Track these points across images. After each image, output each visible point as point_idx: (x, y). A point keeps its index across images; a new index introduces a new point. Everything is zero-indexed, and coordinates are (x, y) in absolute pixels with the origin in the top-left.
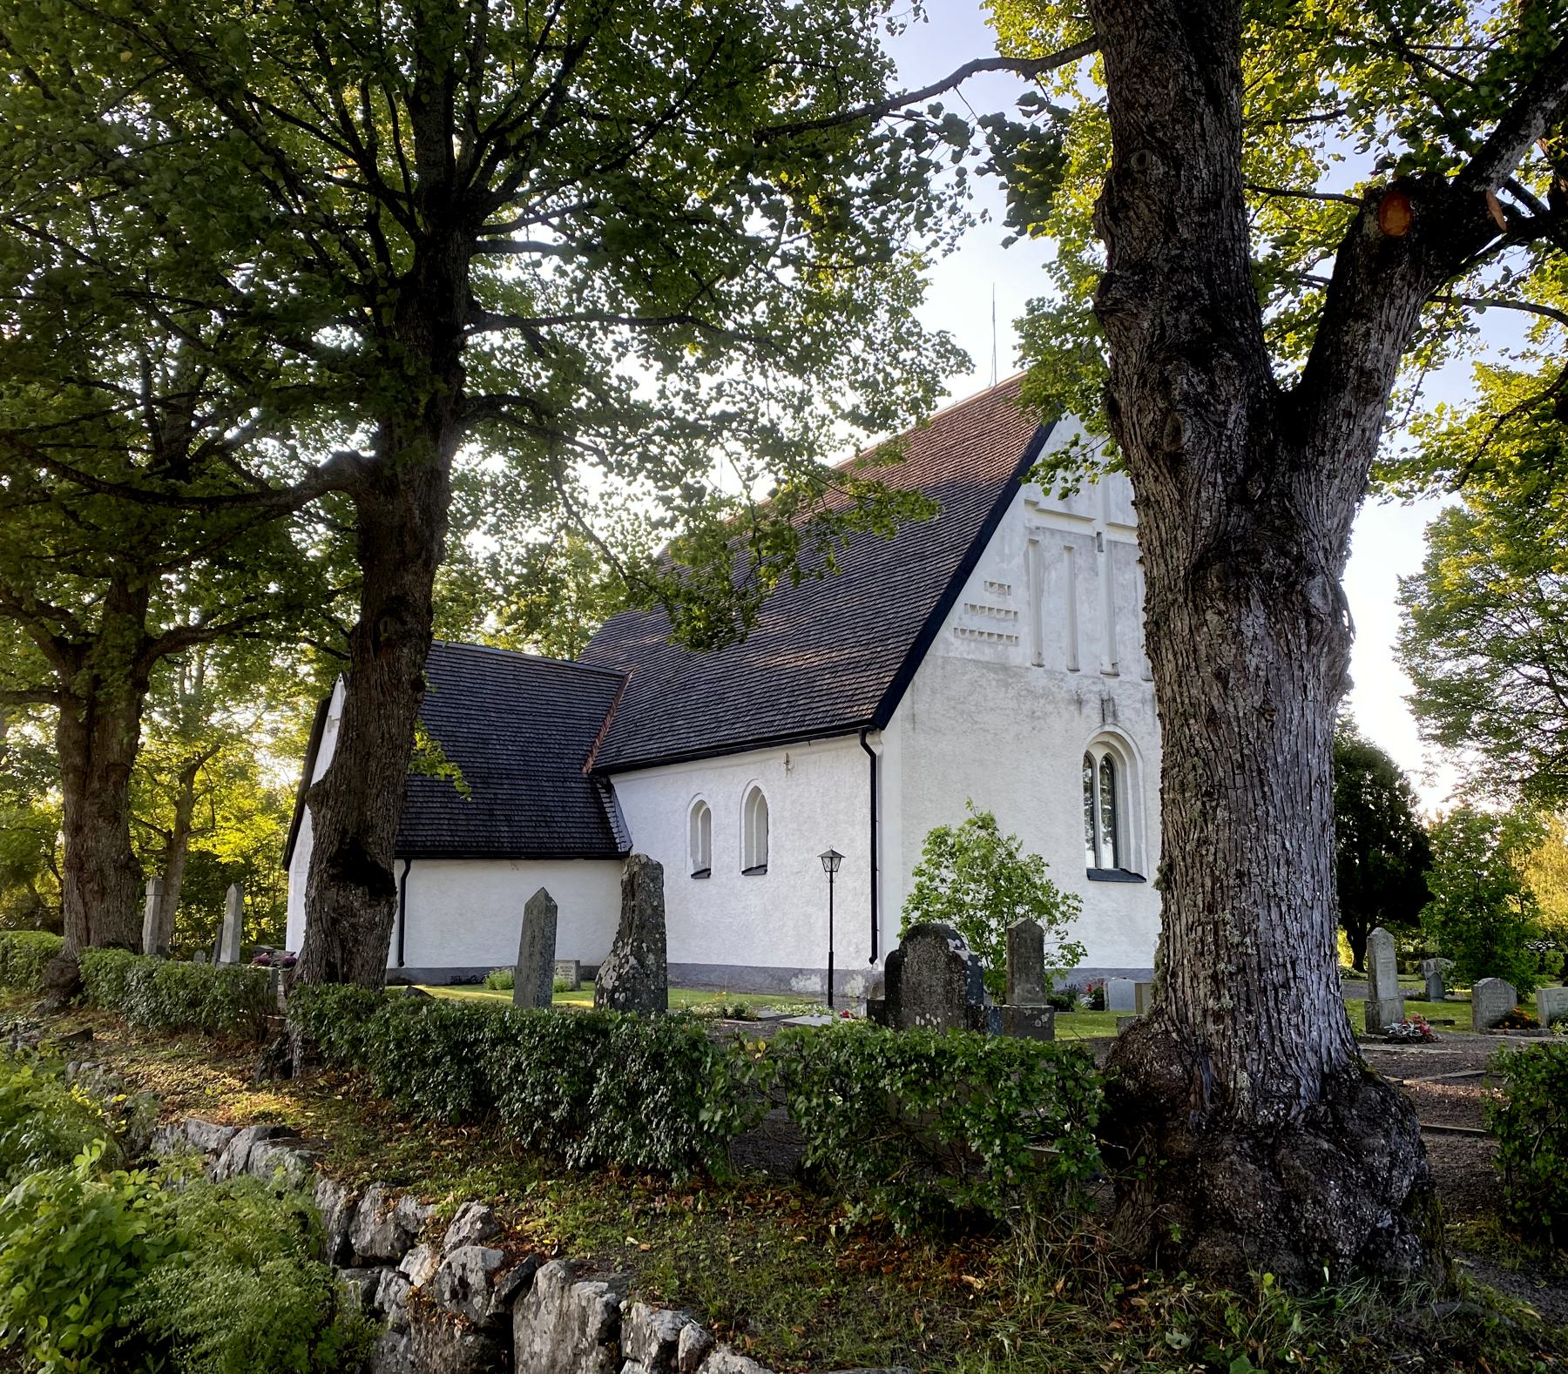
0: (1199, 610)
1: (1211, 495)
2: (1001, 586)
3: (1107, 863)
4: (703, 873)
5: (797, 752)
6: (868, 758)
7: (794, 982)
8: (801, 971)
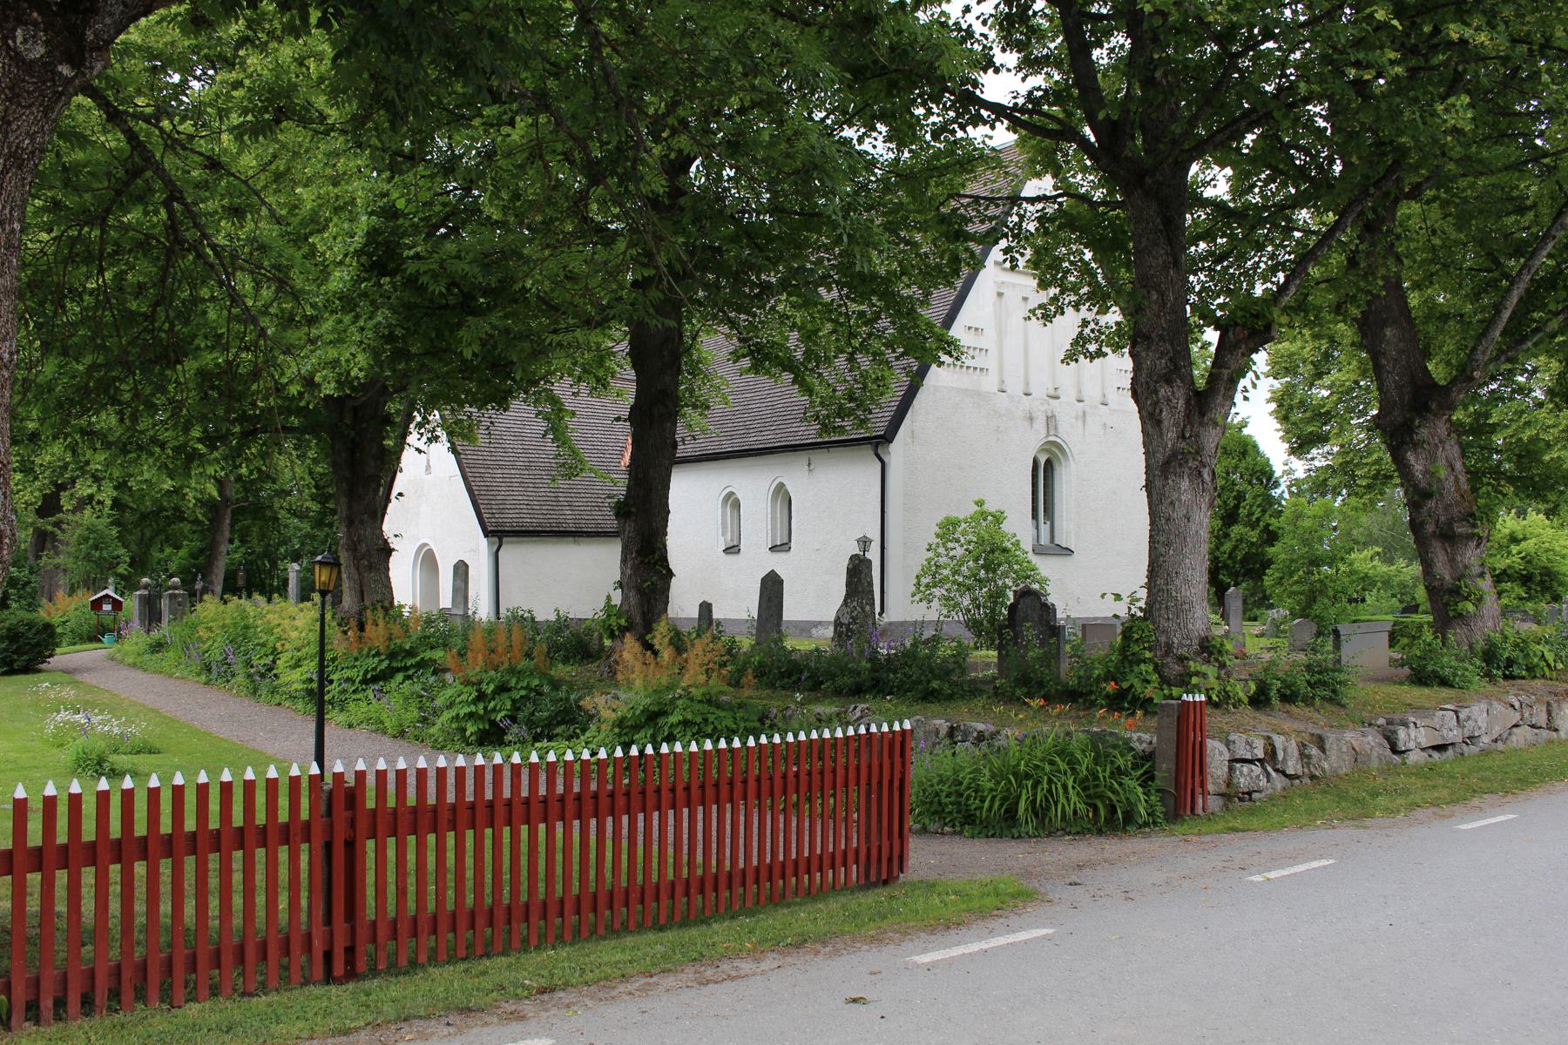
0: (1167, 478)
1: (1171, 435)
2: (977, 329)
3: (1045, 540)
4: (732, 550)
5: (818, 456)
7: (814, 631)
8: (820, 623)
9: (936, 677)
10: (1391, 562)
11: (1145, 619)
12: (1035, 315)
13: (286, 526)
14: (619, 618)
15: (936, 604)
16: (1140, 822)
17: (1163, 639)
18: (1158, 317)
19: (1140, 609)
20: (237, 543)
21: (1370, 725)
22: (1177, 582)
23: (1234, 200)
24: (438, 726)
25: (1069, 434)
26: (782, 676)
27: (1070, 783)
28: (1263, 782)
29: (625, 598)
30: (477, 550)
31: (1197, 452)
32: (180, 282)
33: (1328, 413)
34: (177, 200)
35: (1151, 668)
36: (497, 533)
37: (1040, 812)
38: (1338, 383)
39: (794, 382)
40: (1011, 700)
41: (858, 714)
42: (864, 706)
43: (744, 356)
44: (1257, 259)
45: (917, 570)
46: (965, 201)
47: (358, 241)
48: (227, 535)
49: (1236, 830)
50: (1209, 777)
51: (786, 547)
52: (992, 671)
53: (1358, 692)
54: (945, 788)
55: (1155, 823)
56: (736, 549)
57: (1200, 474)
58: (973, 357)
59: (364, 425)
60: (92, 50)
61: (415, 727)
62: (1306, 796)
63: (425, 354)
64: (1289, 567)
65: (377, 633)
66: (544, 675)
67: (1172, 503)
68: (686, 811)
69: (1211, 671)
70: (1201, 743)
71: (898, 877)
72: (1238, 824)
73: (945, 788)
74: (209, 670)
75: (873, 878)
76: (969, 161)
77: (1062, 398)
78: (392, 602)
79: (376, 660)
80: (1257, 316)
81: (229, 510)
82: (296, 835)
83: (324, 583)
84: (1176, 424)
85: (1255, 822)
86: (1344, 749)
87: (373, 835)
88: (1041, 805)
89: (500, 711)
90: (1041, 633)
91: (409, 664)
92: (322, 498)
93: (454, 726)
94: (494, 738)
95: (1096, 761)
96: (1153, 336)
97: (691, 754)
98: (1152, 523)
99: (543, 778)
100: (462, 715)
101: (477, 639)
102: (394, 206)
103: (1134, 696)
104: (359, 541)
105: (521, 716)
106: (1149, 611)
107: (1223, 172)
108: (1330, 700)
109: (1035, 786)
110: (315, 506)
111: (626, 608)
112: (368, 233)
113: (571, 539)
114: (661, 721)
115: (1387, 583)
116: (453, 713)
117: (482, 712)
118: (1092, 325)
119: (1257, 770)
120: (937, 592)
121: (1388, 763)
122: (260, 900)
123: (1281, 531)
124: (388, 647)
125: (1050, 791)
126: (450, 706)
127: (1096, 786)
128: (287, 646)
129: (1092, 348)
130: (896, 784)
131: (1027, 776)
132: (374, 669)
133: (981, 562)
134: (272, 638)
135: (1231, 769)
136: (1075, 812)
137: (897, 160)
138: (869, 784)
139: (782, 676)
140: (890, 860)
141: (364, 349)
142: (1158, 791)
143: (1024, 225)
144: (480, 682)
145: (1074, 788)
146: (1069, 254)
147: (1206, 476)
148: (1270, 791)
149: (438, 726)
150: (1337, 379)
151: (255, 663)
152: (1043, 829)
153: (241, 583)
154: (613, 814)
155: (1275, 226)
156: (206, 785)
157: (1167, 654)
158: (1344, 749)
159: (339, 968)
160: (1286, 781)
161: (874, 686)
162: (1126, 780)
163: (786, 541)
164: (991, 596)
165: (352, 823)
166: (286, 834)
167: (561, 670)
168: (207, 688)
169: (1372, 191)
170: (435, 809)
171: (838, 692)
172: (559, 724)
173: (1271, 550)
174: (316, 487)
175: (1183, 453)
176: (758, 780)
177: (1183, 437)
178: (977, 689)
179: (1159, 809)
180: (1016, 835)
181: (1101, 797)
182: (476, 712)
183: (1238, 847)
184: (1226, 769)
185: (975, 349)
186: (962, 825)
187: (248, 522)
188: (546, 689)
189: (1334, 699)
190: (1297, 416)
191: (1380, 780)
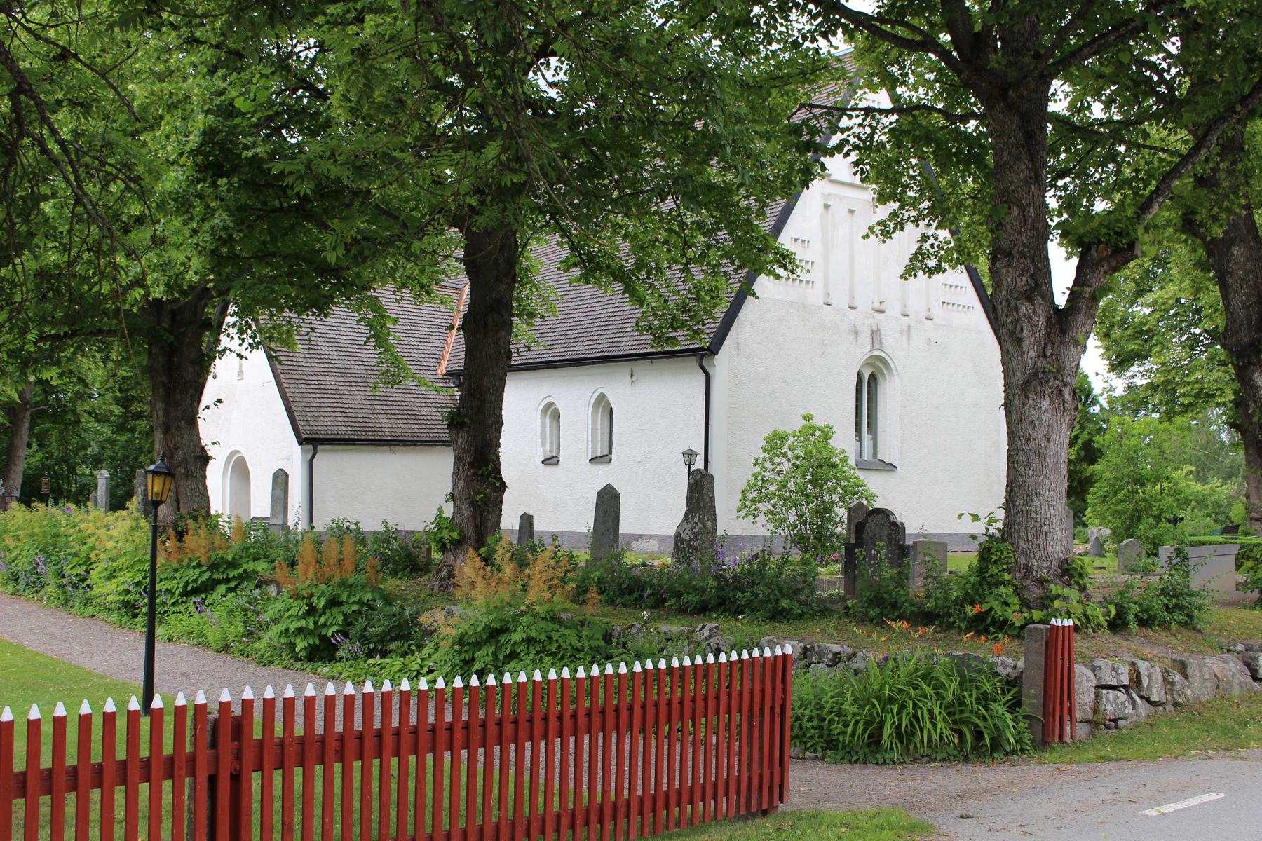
1: (1031, 354)
2: (803, 241)
3: (867, 455)
4: (552, 461)
5: (639, 366)
8: (641, 536)
9: (785, 596)
10: (1203, 481)
12: (873, 232)
13: (86, 430)
14: (452, 530)
15: (762, 519)
17: (1022, 561)
18: (1019, 233)
19: (999, 529)
20: (35, 447)
21: (1229, 651)
22: (1037, 503)
24: (265, 640)
25: (893, 349)
26: (623, 592)
27: (936, 710)
29: (457, 510)
30: (292, 457)
31: (1058, 371)
32: (22, 179)
33: (1150, 330)
34: (24, 92)
35: (1010, 590)
36: (311, 441)
37: (904, 738)
38: (1160, 301)
39: (624, 293)
40: (863, 621)
41: (706, 633)
42: (713, 625)
43: (575, 265)
45: (744, 485)
46: (817, 111)
47: (194, 140)
48: (26, 438)
49: (1109, 759)
52: (839, 590)
53: (1213, 617)
54: (807, 712)
55: (1022, 750)
56: (555, 460)
57: (1061, 393)
58: (808, 271)
59: (182, 330)
61: (240, 642)
62: (1172, 723)
63: (252, 257)
64: (1114, 486)
65: (196, 541)
66: (375, 589)
67: (1032, 423)
68: (572, 739)
69: (1072, 593)
70: (1069, 668)
71: (777, 807)
72: (1108, 751)
73: (807, 712)
74: (17, 580)
75: (754, 809)
76: (813, 71)
77: (887, 313)
78: (208, 512)
79: (197, 571)
80: (1120, 234)
81: (28, 413)
82: (181, 768)
83: (157, 494)
84: (1037, 342)
85: (1126, 751)
86: (1207, 676)
87: (260, 767)
88: (906, 732)
89: (331, 625)
91: (231, 576)
92: (125, 402)
93: (282, 641)
94: (324, 654)
96: (1014, 252)
97: (578, 680)
98: (1011, 442)
99: (431, 705)
100: (291, 630)
103: (993, 618)
104: (176, 448)
105: (352, 631)
106: (1007, 533)
108: (1186, 624)
109: (899, 713)
110: (118, 410)
111: (458, 520)
112: (204, 132)
114: (503, 638)
115: (1201, 502)
116: (282, 627)
117: (312, 627)
118: (932, 241)
119: (1122, 696)
120: (763, 507)
121: (1249, 691)
124: (209, 558)
125: (915, 716)
126: (276, 621)
127: (961, 712)
128: (102, 556)
129: (932, 263)
130: (778, 710)
132: (195, 581)
133: (809, 477)
134: (85, 547)
135: (1097, 695)
136: (942, 738)
138: (751, 710)
140: (771, 788)
141: (200, 252)
142: (1025, 717)
143: (876, 137)
144: (312, 595)
147: (1067, 395)
148: (1135, 718)
149: (265, 640)
150: (1160, 297)
151: (67, 572)
152: (908, 755)
153: (44, 489)
154: (500, 744)
156: (89, 717)
157: (1026, 576)
158: (1207, 676)
160: (1152, 708)
161: (720, 605)
162: (995, 706)
164: (818, 512)
165: (239, 755)
166: (170, 768)
167: (391, 585)
168: (14, 599)
169: (1239, 108)
170: (323, 740)
171: (682, 611)
172: (393, 639)
173: (1096, 467)
174: (120, 390)
175: (1044, 372)
176: (644, 707)
177: (1044, 356)
178: (827, 609)
179: (1027, 736)
180: (881, 761)
182: (306, 628)
184: (1093, 696)
185: (807, 262)
186: (824, 750)
187: (47, 425)
188: (379, 604)
189: (1189, 624)
191: (1243, 709)
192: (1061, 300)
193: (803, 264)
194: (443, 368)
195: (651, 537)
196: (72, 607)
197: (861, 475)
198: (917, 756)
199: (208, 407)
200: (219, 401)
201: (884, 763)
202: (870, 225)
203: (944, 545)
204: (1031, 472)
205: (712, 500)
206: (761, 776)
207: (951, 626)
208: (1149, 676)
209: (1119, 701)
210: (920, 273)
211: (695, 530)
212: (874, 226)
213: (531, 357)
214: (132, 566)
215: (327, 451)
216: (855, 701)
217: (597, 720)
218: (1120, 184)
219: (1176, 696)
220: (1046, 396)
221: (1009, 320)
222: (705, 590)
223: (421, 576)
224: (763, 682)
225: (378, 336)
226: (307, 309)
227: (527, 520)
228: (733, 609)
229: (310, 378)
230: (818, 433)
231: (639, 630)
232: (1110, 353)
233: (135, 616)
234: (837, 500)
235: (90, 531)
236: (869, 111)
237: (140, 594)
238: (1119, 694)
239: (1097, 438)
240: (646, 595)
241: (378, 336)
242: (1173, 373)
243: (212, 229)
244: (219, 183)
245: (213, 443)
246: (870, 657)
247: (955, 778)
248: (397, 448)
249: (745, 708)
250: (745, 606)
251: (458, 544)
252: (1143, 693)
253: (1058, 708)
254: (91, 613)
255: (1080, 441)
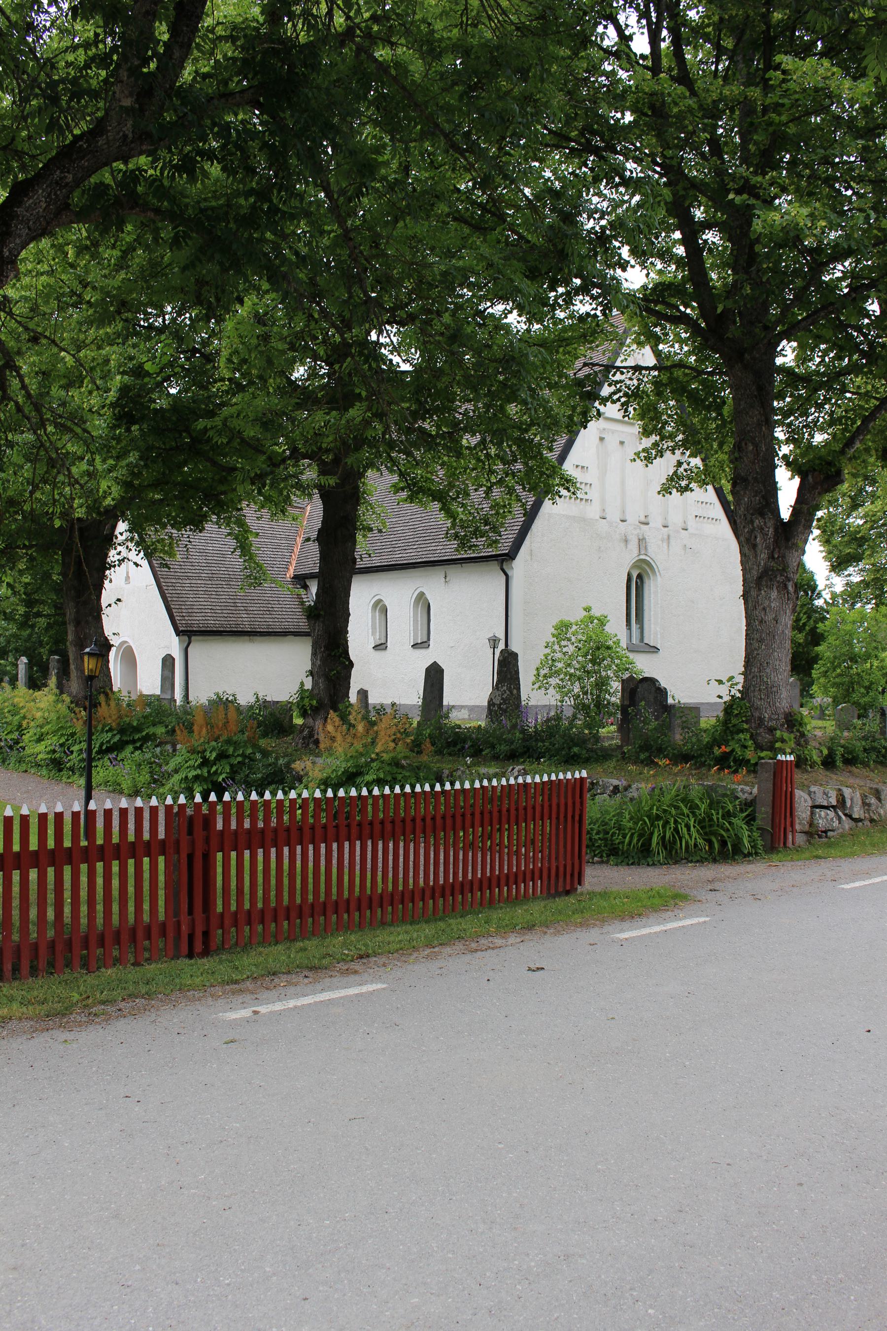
0: (760, 590)
1: (763, 556)
2: (583, 467)
4: (380, 647)
5: (452, 570)
6: (504, 577)
9: (576, 745)
11: (742, 699)
12: (639, 457)
15: (551, 691)
16: (746, 852)
17: (757, 714)
19: (739, 690)
22: (768, 670)
23: (798, 366)
25: (656, 553)
26: (449, 745)
27: (692, 823)
28: (836, 824)
29: (315, 684)
30: (173, 645)
31: (784, 570)
33: (862, 538)
38: (871, 513)
39: (441, 510)
42: (521, 767)
43: (403, 489)
44: (817, 415)
45: (537, 664)
47: (112, 395)
50: (797, 819)
51: (426, 645)
52: (617, 742)
55: (756, 854)
56: (384, 646)
57: (786, 587)
60: (8, 263)
67: (764, 609)
75: (561, 889)
78: (111, 689)
79: (110, 735)
83: (92, 670)
84: (767, 547)
89: (221, 773)
90: (655, 711)
91: (136, 737)
92: (30, 603)
93: (183, 786)
95: (711, 806)
96: (750, 478)
101: (199, 719)
102: (142, 368)
103: (735, 758)
105: (238, 777)
106: (745, 692)
107: (790, 344)
109: (664, 827)
110: (22, 610)
111: (316, 692)
113: (247, 638)
117: (206, 774)
118: (685, 466)
119: (831, 814)
120: (554, 681)
122: (100, 908)
123: (826, 634)
125: (676, 830)
126: (176, 771)
127: (711, 826)
128: (32, 724)
130: (577, 818)
131: (658, 818)
132: (108, 742)
133: (589, 657)
134: (17, 717)
135: (812, 813)
137: (528, 331)
138: (558, 818)
139: (449, 745)
140: (572, 875)
142: (758, 829)
144: (205, 750)
145: (694, 827)
146: (667, 409)
147: (791, 588)
148: (841, 830)
150: (870, 510)
152: (671, 858)
155: (830, 388)
159: (199, 947)
160: (854, 823)
161: (525, 753)
162: (734, 820)
163: (425, 639)
164: (597, 685)
165: (207, 840)
171: (496, 758)
173: (819, 649)
175: (773, 570)
177: (773, 558)
179: (760, 842)
180: (651, 863)
181: (715, 834)
183: (824, 868)
184: (809, 813)
185: (586, 484)
186: (608, 856)
188: (258, 756)
190: (838, 539)
192: (785, 514)
193: (583, 486)
194: (291, 573)
195: (462, 707)
196: (9, 764)
197: (631, 656)
198: (678, 859)
199: (110, 605)
200: (119, 600)
201: (654, 864)
202: (636, 451)
203: (699, 708)
204: (763, 647)
205: (517, 672)
206: (565, 866)
207: (703, 764)
208: (852, 799)
209: (829, 818)
210: (674, 491)
211: (504, 696)
212: (639, 453)
213: (376, 562)
214: (58, 730)
215: (199, 641)
216: (631, 818)
217: (449, 822)
218: (832, 422)
219: (872, 814)
220: (775, 588)
221: (746, 530)
222: (514, 741)
223: (287, 736)
224: (566, 798)
225: (244, 547)
226: (185, 526)
227: (363, 694)
228: (536, 756)
229: (185, 581)
230: (596, 621)
231: (463, 772)
232: (831, 556)
233: (60, 770)
234: (612, 675)
235: (21, 705)
236: (637, 368)
237: (65, 752)
238: (829, 812)
239: (820, 625)
240: (467, 746)
241: (244, 547)
242: (881, 572)
243: (127, 465)
244: (133, 429)
245: (114, 634)
246: (641, 788)
247: (707, 872)
248: (255, 638)
249: (554, 816)
250: (544, 753)
251: (316, 710)
252: (847, 812)
253: (783, 821)
254: (24, 769)
255: (807, 628)
